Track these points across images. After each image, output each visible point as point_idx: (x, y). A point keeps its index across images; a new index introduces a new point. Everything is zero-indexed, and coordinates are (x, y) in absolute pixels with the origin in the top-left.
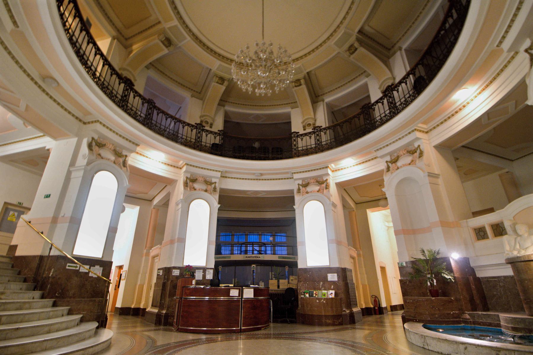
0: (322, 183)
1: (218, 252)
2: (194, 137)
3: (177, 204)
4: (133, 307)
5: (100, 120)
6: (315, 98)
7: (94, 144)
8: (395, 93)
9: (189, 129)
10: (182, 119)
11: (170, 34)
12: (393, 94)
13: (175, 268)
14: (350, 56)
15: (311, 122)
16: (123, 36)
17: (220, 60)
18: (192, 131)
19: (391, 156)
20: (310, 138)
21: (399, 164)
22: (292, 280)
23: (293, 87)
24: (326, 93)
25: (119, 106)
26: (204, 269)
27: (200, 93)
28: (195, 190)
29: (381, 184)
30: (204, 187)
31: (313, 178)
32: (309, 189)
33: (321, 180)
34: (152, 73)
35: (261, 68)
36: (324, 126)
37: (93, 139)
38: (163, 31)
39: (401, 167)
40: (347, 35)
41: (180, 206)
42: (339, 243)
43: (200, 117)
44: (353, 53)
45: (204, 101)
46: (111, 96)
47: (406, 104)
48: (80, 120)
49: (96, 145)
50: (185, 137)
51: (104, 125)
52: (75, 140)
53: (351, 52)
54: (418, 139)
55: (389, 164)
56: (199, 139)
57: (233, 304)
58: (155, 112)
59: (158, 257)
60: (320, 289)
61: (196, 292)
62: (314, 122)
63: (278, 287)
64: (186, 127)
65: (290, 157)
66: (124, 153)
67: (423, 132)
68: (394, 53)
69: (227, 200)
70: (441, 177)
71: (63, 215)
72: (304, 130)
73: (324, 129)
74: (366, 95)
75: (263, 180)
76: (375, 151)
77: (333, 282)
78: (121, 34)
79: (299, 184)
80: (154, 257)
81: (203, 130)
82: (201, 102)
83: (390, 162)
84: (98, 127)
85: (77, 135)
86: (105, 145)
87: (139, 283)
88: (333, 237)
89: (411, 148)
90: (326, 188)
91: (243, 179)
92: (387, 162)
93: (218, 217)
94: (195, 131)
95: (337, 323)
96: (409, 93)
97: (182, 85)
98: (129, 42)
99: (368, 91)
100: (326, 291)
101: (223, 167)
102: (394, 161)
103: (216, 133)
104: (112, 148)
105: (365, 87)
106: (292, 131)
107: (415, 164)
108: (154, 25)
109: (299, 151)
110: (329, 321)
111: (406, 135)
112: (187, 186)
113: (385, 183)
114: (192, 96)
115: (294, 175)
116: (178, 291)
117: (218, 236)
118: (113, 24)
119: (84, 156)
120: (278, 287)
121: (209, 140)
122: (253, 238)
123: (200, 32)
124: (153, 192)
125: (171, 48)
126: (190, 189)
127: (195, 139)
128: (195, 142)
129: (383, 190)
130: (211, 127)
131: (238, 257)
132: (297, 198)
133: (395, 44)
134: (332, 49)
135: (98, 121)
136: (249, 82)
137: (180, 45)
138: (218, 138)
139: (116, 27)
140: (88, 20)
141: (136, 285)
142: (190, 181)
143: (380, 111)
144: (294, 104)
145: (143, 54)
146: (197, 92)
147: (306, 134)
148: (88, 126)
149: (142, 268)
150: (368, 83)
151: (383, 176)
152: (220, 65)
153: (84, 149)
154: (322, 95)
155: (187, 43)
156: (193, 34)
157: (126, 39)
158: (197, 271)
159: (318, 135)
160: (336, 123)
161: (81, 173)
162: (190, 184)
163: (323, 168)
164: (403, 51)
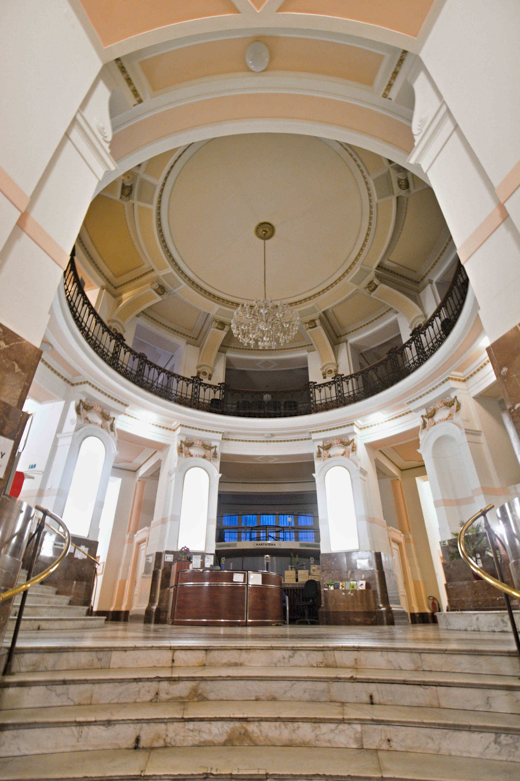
0: (348, 444)
1: (220, 538)
2: (190, 392)
3: (170, 474)
4: (112, 609)
5: (89, 381)
6: (336, 339)
7: (82, 407)
8: (422, 336)
9: (185, 383)
10: (175, 372)
11: (165, 282)
12: (420, 337)
13: (167, 552)
14: (370, 294)
15: (333, 368)
16: (112, 285)
17: (220, 304)
18: (187, 386)
19: (426, 409)
20: (330, 389)
21: (436, 418)
22: (314, 570)
23: (307, 329)
24: (350, 332)
25: (110, 365)
26: (203, 555)
27: (196, 339)
28: (191, 456)
29: (416, 444)
30: (202, 452)
31: (337, 438)
32: (332, 452)
33: (347, 441)
34: (142, 321)
35: (263, 322)
36: (345, 375)
37: (81, 401)
38: (158, 279)
39: (437, 422)
40: (364, 272)
41: (174, 476)
42: (371, 520)
43: (197, 368)
44: (374, 290)
45: (201, 350)
46: (102, 355)
47: (434, 350)
48: (68, 382)
49: (84, 408)
50: (180, 394)
51: (93, 386)
52: (61, 404)
53: (371, 289)
54: (453, 389)
55: (425, 419)
56: (195, 394)
57: (237, 591)
58: (147, 367)
59: (145, 543)
60: (348, 580)
61: (197, 576)
62: (335, 368)
63: (297, 580)
64: (181, 382)
65: (308, 412)
66: (112, 415)
67: (459, 380)
68: (424, 287)
69: (232, 469)
70: (483, 433)
71: (49, 487)
72: (325, 378)
73: (347, 378)
74: (396, 335)
75: (274, 441)
76: (407, 403)
77: (364, 571)
78: (110, 282)
79: (319, 446)
80: (139, 544)
81: (201, 384)
82: (198, 349)
83: (426, 417)
84: (87, 388)
85: (64, 399)
86: (92, 408)
87: (120, 578)
88: (363, 512)
89: (448, 400)
90: (353, 451)
91: (250, 441)
92: (422, 416)
93: (219, 492)
94: (191, 385)
95: (368, 623)
96: (436, 337)
97: (175, 331)
98: (119, 290)
99: (398, 330)
100: (355, 582)
101: (225, 427)
102: (431, 415)
103: (215, 387)
104: (100, 411)
105: (395, 325)
106: (310, 381)
107: (452, 420)
108: (147, 273)
109: (316, 405)
110: (358, 620)
111: (440, 385)
112: (182, 452)
113: (420, 442)
114: (187, 343)
115: (312, 434)
116: (173, 582)
117: (220, 516)
118: (103, 274)
119: (72, 421)
120: (297, 580)
121: (207, 395)
122: (269, 520)
123: (197, 276)
124: (138, 461)
125: (165, 296)
126: (185, 455)
127: (192, 396)
128: (191, 399)
129: (419, 451)
130: (210, 379)
131: (246, 545)
132: (318, 464)
133: (424, 277)
134: (348, 287)
135: (87, 382)
136: (251, 336)
137: (176, 290)
139: (105, 277)
140: (82, 279)
141: (115, 582)
142: (428, 418)
143: (411, 354)
144: (310, 347)
145: (133, 303)
147: (324, 385)
148: (76, 387)
149: (124, 558)
150: (398, 319)
151: (418, 436)
152: (220, 309)
153: (72, 413)
154: (344, 335)
155: (183, 290)
156: (189, 279)
157: (116, 288)
158: (194, 556)
159: (339, 385)
160: (367, 367)
161: (69, 440)
162: (185, 449)
163: (348, 425)
164: (434, 285)
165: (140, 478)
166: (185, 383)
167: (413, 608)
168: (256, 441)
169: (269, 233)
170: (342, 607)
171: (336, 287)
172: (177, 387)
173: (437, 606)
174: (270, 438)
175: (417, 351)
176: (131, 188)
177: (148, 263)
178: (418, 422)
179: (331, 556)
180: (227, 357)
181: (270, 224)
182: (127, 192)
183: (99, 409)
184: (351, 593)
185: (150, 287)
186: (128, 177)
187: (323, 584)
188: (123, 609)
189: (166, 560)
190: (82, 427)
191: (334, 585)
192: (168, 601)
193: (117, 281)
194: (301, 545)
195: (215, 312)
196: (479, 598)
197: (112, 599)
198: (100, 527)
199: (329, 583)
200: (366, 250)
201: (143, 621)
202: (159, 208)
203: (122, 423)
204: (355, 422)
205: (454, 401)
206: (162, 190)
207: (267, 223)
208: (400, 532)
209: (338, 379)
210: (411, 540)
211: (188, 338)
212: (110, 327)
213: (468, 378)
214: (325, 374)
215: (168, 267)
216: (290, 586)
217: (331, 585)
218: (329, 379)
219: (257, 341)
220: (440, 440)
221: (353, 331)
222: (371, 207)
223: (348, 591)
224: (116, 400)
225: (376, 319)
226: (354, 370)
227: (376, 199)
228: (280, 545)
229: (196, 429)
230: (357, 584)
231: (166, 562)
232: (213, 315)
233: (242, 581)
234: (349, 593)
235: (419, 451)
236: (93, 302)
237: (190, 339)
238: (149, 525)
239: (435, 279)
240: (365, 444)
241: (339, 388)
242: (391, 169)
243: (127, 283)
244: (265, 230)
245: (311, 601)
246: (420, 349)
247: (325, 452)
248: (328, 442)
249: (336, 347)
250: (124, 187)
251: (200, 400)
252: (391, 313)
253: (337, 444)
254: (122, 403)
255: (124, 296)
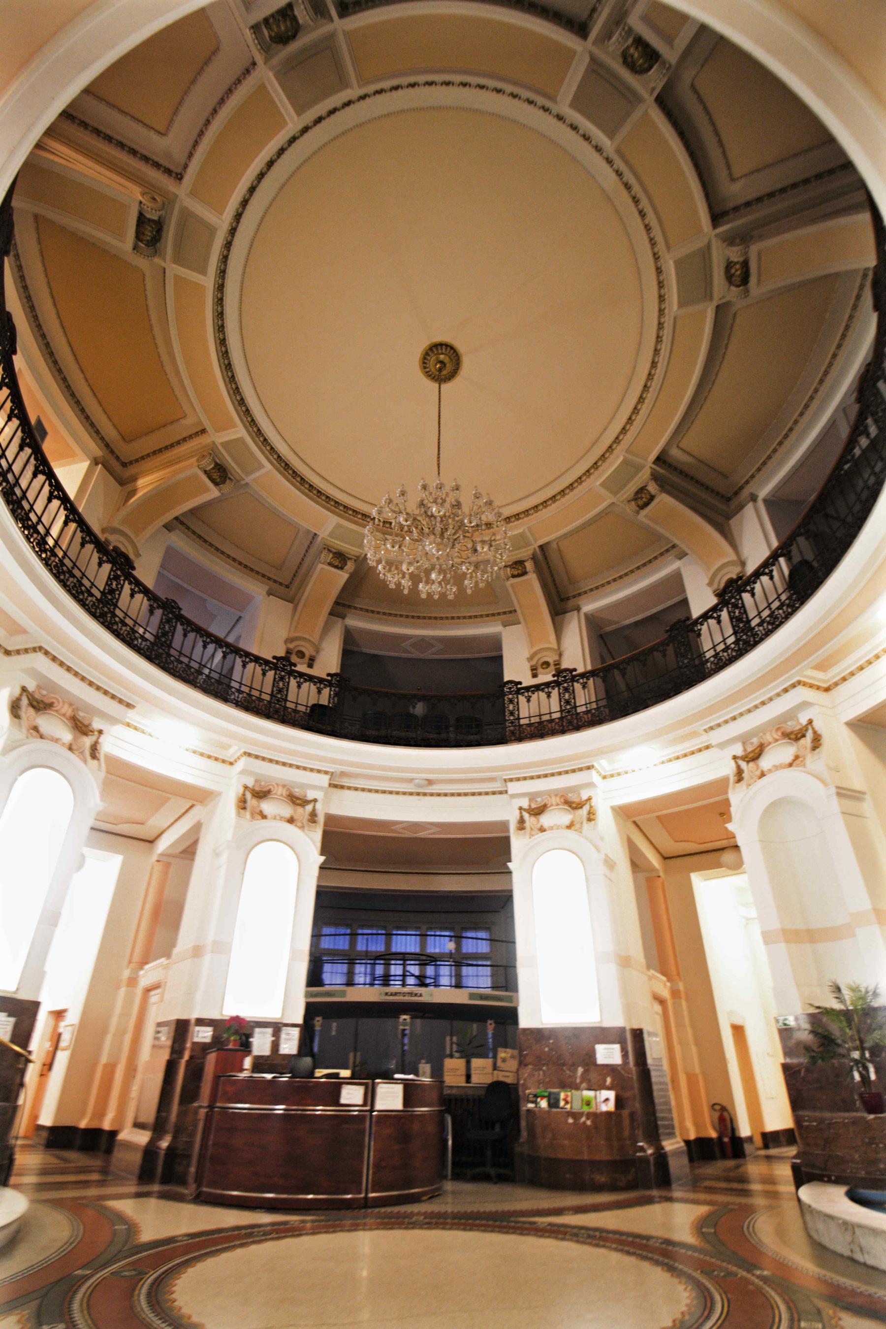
0: (579, 806)
1: (314, 978)
3: (217, 855)
4: (83, 1124)
6: (560, 603)
8: (746, 596)
9: (259, 670)
10: (242, 645)
12: (741, 598)
13: (200, 1022)
14: (638, 513)
16: (117, 458)
18: (264, 674)
19: (744, 743)
20: (549, 696)
21: (765, 762)
23: (508, 579)
24: (586, 592)
26: (277, 1028)
28: (264, 817)
29: (723, 811)
30: (287, 810)
31: (556, 793)
32: (546, 820)
33: (577, 800)
34: (178, 540)
36: (581, 670)
38: (212, 451)
40: (630, 467)
41: (224, 858)
42: (625, 962)
44: (646, 505)
46: (77, 590)
47: (774, 623)
53: (640, 503)
56: (279, 693)
57: (349, 1125)
60: (577, 1088)
62: (557, 658)
66: (97, 724)
67: (818, 688)
68: (741, 507)
69: (343, 844)
70: (867, 797)
72: (535, 676)
73: (582, 675)
75: (432, 795)
76: (705, 731)
78: (112, 452)
79: (521, 809)
80: (148, 990)
81: (291, 673)
83: (743, 758)
84: (40, 662)
87: (104, 1060)
89: (791, 726)
90: (589, 820)
92: (735, 758)
93: (318, 886)
94: (271, 674)
98: (132, 470)
103: (321, 680)
105: (676, 581)
106: (506, 679)
107: (804, 766)
112: (244, 808)
114: (270, 593)
115: (509, 784)
117: (316, 936)
118: (98, 432)
120: (468, 1077)
121: (304, 695)
124: (157, 821)
125: (227, 487)
127: (272, 695)
129: (730, 827)
130: (310, 666)
132: (517, 844)
133: (741, 488)
134: (597, 497)
135: (41, 648)
138: (326, 692)
139: (102, 439)
140: (39, 422)
141: (94, 1065)
142: (748, 762)
144: (509, 616)
145: (161, 497)
146: (281, 584)
147: (537, 688)
151: (727, 793)
152: (338, 526)
154: (574, 597)
155: (265, 477)
159: (566, 690)
162: (251, 802)
165: (161, 855)
166: (259, 670)
167: (687, 1130)
168: (397, 793)
169: (449, 367)
170: (567, 1150)
171: (571, 496)
172: (246, 676)
173: (728, 1122)
174: (425, 789)
175: (733, 627)
176: (159, 226)
177: (196, 413)
178: (728, 769)
179: (538, 1034)
180: (346, 626)
181: (452, 348)
182: (148, 234)
183: (67, 710)
184: (588, 1119)
185: (196, 464)
186: (154, 199)
187: (524, 1092)
188: (107, 1125)
189: (196, 1040)
190: (20, 746)
191: (549, 1097)
192: (192, 1135)
193: (128, 451)
194: (472, 996)
195: (327, 533)
196: (880, 1156)
197: (85, 1104)
198: (48, 967)
199: (539, 1091)
200: (639, 420)
201: (135, 1182)
202: (220, 288)
203: (117, 742)
204: (595, 764)
205: (807, 730)
206: (228, 245)
207: (447, 345)
208: (664, 978)
209: (565, 677)
210: (683, 995)
211: (271, 583)
212: (107, 542)
213: (836, 684)
214: (536, 669)
215: (234, 426)
216: (454, 1091)
217: (543, 1097)
218: (546, 677)
219: (415, 579)
220: (774, 808)
221: (591, 590)
222: (660, 326)
223: (581, 1114)
224: (106, 693)
225: (638, 568)
226: (592, 664)
227: (675, 307)
228: (431, 995)
229: (277, 762)
230: (596, 1097)
231: (194, 1044)
232: (323, 538)
233: (360, 1102)
234: (583, 1119)
235: (730, 827)
236: (71, 486)
237: (276, 586)
238: (168, 955)
239: (764, 492)
240: (613, 809)
241: (567, 696)
242: (714, 240)
243: (148, 455)
244: (442, 362)
245: (497, 1128)
246: (741, 623)
247: (533, 819)
248: (539, 799)
249: (558, 618)
250: (142, 220)
251: (289, 705)
252: (669, 557)
253: (558, 805)
254: (121, 701)
255: (141, 482)
